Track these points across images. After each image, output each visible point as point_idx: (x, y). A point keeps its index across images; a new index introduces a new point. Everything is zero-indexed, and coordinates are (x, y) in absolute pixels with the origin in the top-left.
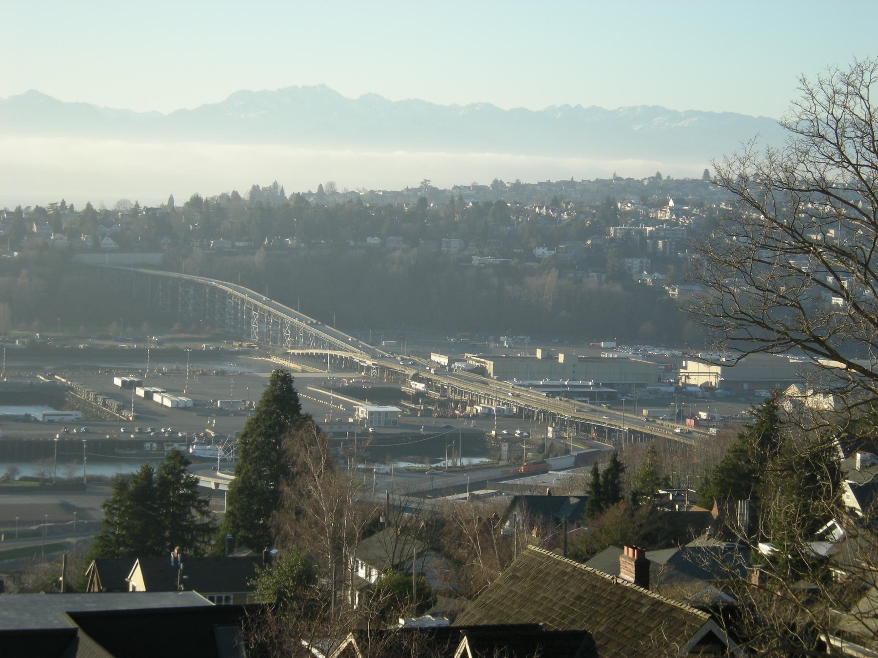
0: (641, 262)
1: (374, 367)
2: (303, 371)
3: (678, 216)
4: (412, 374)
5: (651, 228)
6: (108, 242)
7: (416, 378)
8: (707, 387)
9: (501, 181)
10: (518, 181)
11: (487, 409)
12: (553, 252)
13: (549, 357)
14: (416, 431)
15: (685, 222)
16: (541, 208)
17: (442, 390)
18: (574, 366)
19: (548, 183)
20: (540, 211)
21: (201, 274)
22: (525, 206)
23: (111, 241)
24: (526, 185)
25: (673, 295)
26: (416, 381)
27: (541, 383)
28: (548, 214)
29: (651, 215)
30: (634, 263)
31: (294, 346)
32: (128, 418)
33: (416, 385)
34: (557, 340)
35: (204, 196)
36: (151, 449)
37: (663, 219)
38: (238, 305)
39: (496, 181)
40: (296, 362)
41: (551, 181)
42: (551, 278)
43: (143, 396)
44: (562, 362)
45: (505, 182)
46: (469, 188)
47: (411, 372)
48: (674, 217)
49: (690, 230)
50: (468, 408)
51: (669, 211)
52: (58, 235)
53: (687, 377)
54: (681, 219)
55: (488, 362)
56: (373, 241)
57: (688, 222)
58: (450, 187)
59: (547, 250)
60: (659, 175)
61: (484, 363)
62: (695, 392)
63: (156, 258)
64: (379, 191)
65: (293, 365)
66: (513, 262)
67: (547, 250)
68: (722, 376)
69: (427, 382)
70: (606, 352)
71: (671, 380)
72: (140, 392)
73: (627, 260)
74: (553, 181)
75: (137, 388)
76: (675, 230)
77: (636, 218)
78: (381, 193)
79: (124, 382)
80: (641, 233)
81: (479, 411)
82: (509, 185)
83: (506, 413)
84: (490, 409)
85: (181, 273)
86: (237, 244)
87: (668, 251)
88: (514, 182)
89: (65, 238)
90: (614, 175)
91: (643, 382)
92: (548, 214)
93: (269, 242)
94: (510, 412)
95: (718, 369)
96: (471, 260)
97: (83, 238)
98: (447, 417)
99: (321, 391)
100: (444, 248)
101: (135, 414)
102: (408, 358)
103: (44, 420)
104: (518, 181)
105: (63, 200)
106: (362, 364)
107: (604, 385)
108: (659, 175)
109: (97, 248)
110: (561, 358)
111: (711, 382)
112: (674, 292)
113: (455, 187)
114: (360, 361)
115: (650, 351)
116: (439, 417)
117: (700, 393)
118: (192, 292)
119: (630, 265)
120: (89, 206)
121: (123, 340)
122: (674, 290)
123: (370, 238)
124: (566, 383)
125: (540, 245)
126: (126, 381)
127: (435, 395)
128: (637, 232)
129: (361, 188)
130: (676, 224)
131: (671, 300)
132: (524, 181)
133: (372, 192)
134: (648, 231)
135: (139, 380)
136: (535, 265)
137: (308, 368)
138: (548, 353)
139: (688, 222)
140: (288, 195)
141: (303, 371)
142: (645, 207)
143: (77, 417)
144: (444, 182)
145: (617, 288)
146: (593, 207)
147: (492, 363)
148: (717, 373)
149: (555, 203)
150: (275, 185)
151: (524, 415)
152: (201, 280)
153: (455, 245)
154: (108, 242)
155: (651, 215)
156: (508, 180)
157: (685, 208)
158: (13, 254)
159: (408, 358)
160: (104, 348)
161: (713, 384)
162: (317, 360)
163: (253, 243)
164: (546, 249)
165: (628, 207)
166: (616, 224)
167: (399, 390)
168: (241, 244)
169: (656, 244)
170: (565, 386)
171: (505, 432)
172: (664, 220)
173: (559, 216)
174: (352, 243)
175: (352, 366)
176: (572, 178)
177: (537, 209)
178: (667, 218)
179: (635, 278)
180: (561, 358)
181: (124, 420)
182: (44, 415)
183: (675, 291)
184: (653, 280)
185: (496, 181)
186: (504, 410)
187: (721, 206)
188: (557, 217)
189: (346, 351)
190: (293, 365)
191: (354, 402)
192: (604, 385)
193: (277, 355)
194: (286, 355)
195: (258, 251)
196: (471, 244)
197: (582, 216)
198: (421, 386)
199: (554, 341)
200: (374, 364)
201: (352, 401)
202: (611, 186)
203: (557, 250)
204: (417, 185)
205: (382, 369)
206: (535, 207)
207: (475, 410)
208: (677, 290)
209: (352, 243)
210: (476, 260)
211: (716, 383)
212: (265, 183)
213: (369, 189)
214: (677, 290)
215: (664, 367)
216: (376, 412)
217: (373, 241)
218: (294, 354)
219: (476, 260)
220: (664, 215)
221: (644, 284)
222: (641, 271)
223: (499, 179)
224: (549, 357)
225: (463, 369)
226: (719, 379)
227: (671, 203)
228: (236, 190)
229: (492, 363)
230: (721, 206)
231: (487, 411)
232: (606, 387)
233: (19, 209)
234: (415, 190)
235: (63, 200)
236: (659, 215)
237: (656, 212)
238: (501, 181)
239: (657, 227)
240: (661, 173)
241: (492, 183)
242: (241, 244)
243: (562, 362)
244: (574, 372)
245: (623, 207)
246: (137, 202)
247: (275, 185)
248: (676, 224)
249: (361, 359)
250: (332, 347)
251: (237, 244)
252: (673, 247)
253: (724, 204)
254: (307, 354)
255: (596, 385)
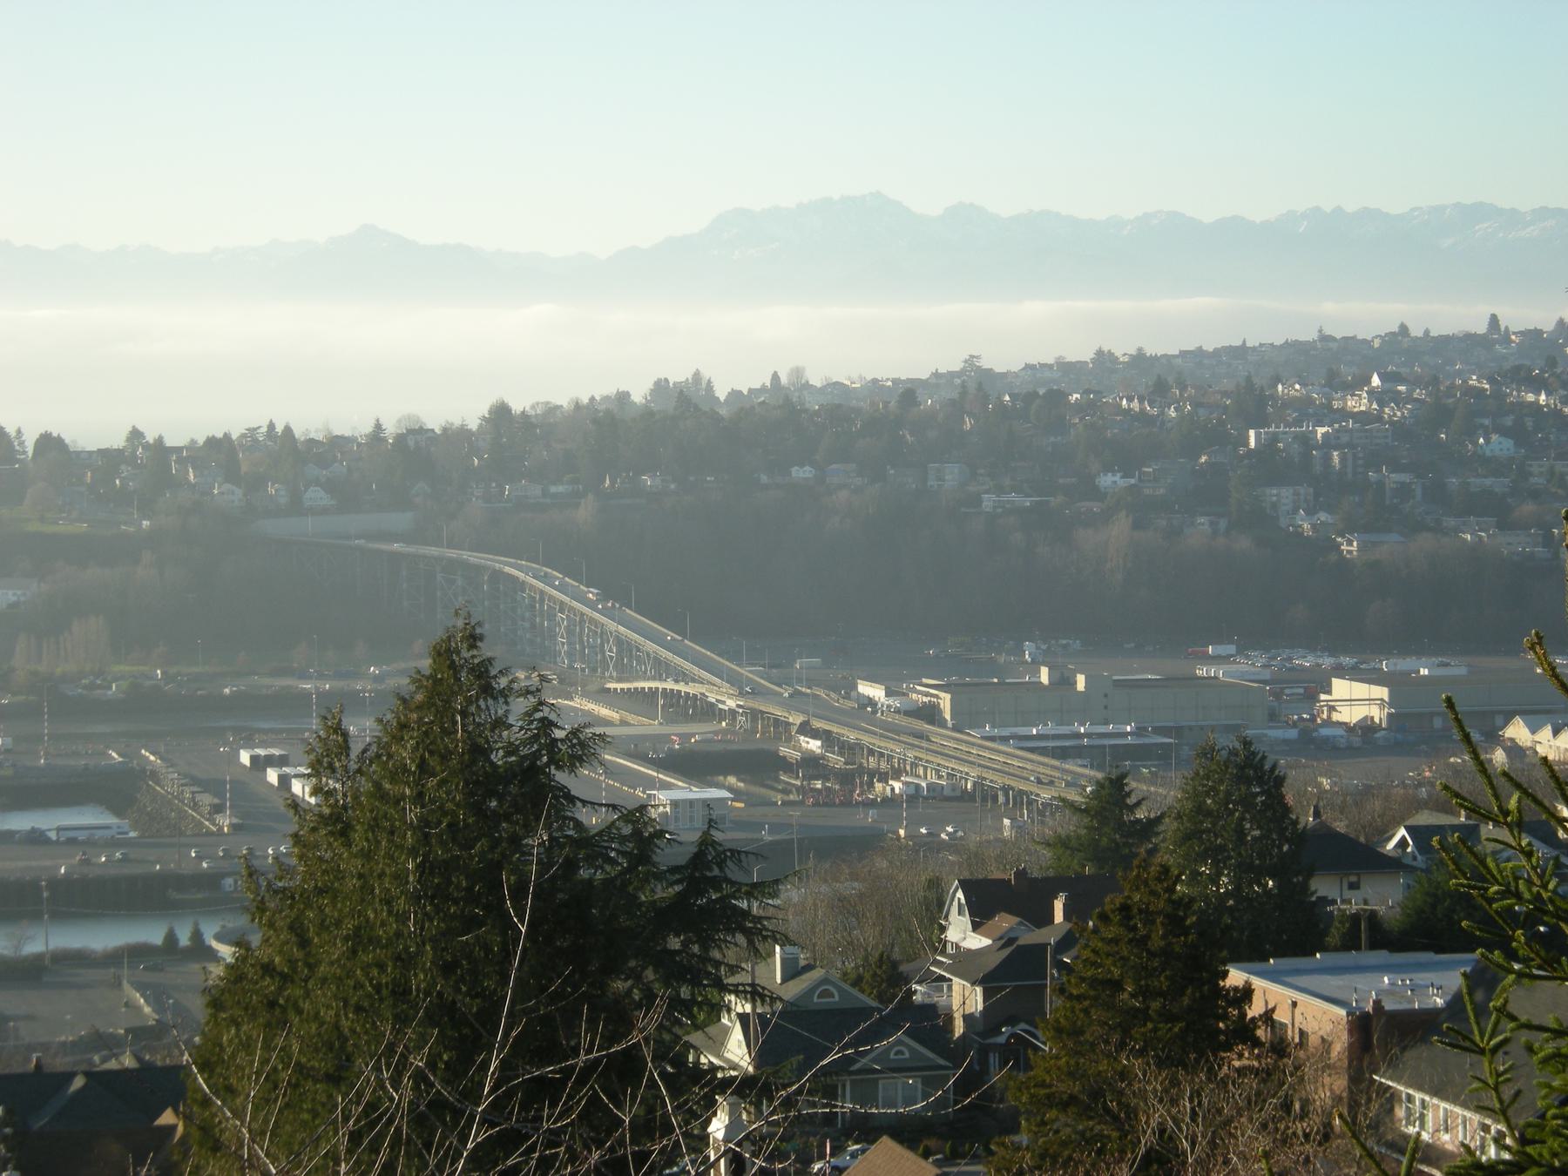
0: (1296, 494)
1: (741, 711)
2: (624, 723)
3: (1382, 404)
4: (798, 722)
5: (1323, 430)
6: (315, 496)
7: (806, 729)
8: (1367, 727)
9: (1109, 351)
10: (1140, 349)
11: (912, 787)
12: (1133, 481)
13: (1063, 682)
14: (755, 836)
15: (1395, 415)
16: (1130, 399)
17: (848, 749)
18: (1106, 696)
19: (1199, 353)
20: (1129, 405)
21: (477, 548)
22: (1104, 397)
23: (322, 494)
24: (1155, 359)
25: (1350, 552)
26: (806, 736)
27: (1034, 732)
28: (1142, 410)
29: (1336, 405)
30: (1281, 496)
31: (624, 674)
32: (221, 828)
33: (808, 743)
34: (1133, 645)
35: (517, 406)
36: (236, 888)
37: (1356, 410)
38: (535, 601)
39: (1100, 353)
40: (610, 706)
41: (1204, 348)
42: (1119, 530)
43: (276, 784)
44: (1083, 689)
45: (1118, 353)
46: (1050, 367)
47: (796, 719)
48: (1375, 406)
49: (1399, 428)
50: (879, 786)
51: (1365, 395)
52: (227, 486)
53: (1332, 709)
54: (1387, 410)
55: (942, 695)
56: (802, 473)
57: (1399, 414)
58: (1016, 366)
59: (1122, 477)
60: (1404, 329)
61: (937, 696)
62: (1334, 737)
63: (401, 520)
64: (888, 379)
65: (604, 712)
66: (1056, 501)
67: (1122, 477)
68: (1391, 707)
69: (827, 738)
70: (1205, 665)
71: (1305, 716)
72: (272, 776)
73: (1268, 491)
74: (1209, 347)
75: (268, 770)
76: (1371, 430)
77: (1307, 411)
78: (890, 383)
79: (254, 759)
80: (1306, 441)
81: (897, 791)
82: (1126, 359)
83: (947, 792)
84: (918, 786)
85: (442, 547)
86: (553, 489)
87: (1349, 470)
88: (1134, 353)
89: (239, 492)
90: (1320, 331)
91: (1239, 722)
92: (1142, 410)
93: (613, 482)
94: (953, 790)
95: (1382, 692)
96: (980, 502)
97: (271, 490)
98: (834, 805)
99: (622, 761)
100: (932, 482)
101: (235, 821)
102: (809, 691)
103: (58, 840)
104: (1140, 349)
105: (271, 421)
106: (721, 706)
107: (1158, 731)
108: (1404, 329)
109: (296, 507)
110: (1081, 682)
111: (1372, 718)
112: (1350, 547)
113: (1028, 367)
114: (717, 700)
115: (1297, 659)
116: (816, 804)
117: (1343, 740)
118: (460, 582)
119: (1275, 498)
120: (1427, 332)
121: (304, 676)
122: (1350, 543)
123: (796, 468)
124: (1082, 730)
125: (1108, 468)
126: (259, 756)
127: (836, 760)
128: (1296, 437)
129: (855, 376)
130: (1379, 418)
131: (1344, 563)
132: (1150, 350)
133: (875, 381)
134: (1319, 436)
135: (283, 753)
136: (1096, 507)
137: (631, 718)
138: (1062, 673)
139: (1399, 414)
140: (721, 393)
141: (624, 723)
142: (1327, 389)
143: (120, 830)
144: (1004, 358)
145: (1244, 543)
146: (1226, 394)
147: (948, 697)
148: (1382, 700)
149: (1160, 391)
150: (697, 376)
151: (984, 796)
152: (474, 558)
153: (952, 475)
154: (315, 496)
155: (1336, 405)
156: (1122, 348)
157: (1399, 388)
158: (141, 524)
159: (809, 691)
160: (269, 692)
161: (1377, 720)
162: (644, 701)
163: (580, 487)
164: (1119, 475)
165: (1296, 390)
166: (1260, 422)
167: (776, 754)
168: (561, 489)
169: (1328, 458)
170: (1079, 736)
171: (923, 831)
172: (1357, 412)
173: (1162, 413)
174: (764, 478)
175: (708, 711)
176: (1244, 341)
177: (1124, 402)
178: (1363, 408)
179: (1283, 522)
180: (1081, 682)
181: (211, 834)
182: (59, 829)
183: (1352, 545)
184: (1314, 526)
185: (1100, 353)
186: (942, 786)
187: (1471, 382)
188: (1158, 416)
189: (702, 683)
190: (604, 712)
191: (672, 781)
192: (1158, 731)
193: (586, 695)
194: (604, 695)
195: (583, 501)
196: (982, 471)
197: (1201, 411)
198: (814, 745)
199: (1126, 646)
200: (739, 706)
201: (668, 779)
202: (1312, 352)
203: (1140, 477)
204: (957, 366)
205: (754, 715)
206: (1121, 399)
207: (888, 788)
208: (1355, 544)
209: (764, 478)
210: (988, 502)
211: (1381, 719)
212: (678, 374)
213: (869, 378)
214: (1355, 544)
215: (1301, 691)
216: (684, 801)
217: (802, 473)
218: (616, 689)
219: (988, 502)
220: (1359, 403)
221: (1299, 534)
222: (1295, 511)
223: (1105, 349)
224: (1063, 682)
225: (898, 711)
226: (1386, 710)
227: (1376, 381)
228: (706, 374)
229: (948, 697)
230: (1471, 382)
231: (912, 791)
232: (1159, 734)
233: (501, 412)
234: (952, 375)
235: (271, 421)
236: (1349, 403)
237: (1344, 399)
238: (1109, 351)
239: (1336, 426)
240: (1408, 325)
241: (1093, 356)
242: (561, 489)
243: (1083, 689)
244: (1106, 707)
245: (1286, 391)
246: (378, 420)
247: (697, 376)
248: (1379, 418)
249: (719, 698)
250: (681, 676)
251: (553, 489)
252: (1360, 462)
253: (1474, 377)
254: (636, 689)
255: (1139, 732)
